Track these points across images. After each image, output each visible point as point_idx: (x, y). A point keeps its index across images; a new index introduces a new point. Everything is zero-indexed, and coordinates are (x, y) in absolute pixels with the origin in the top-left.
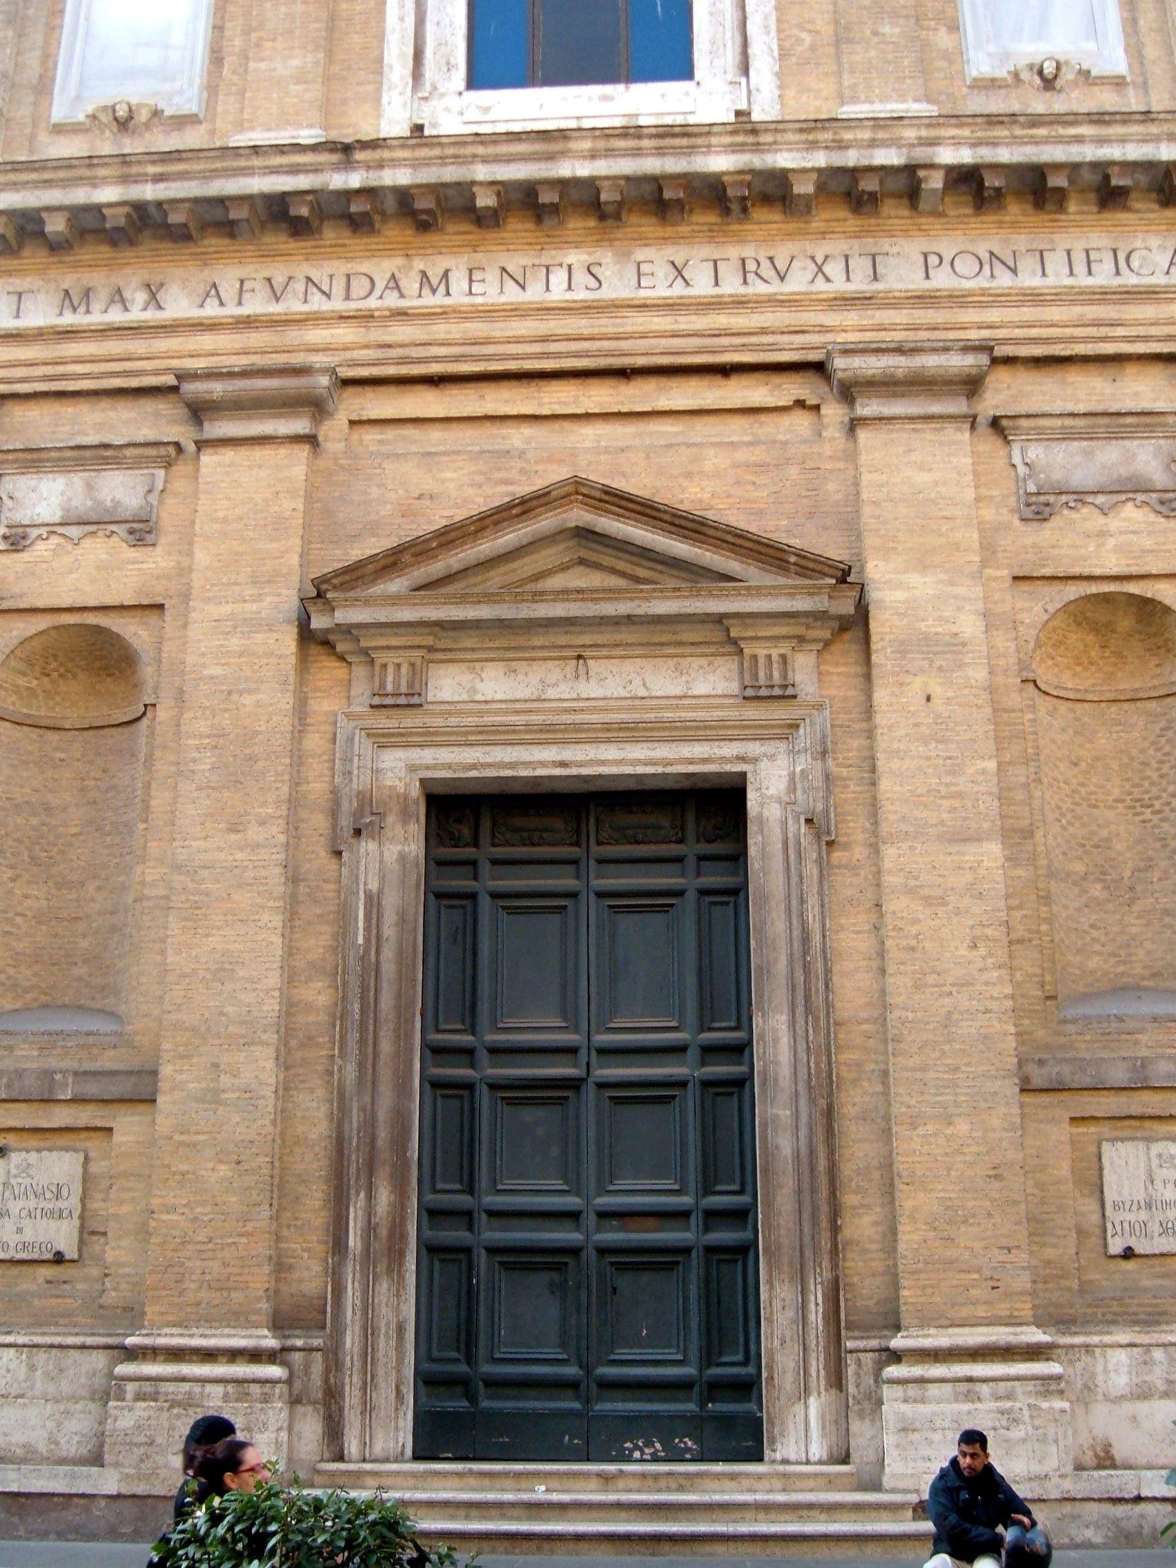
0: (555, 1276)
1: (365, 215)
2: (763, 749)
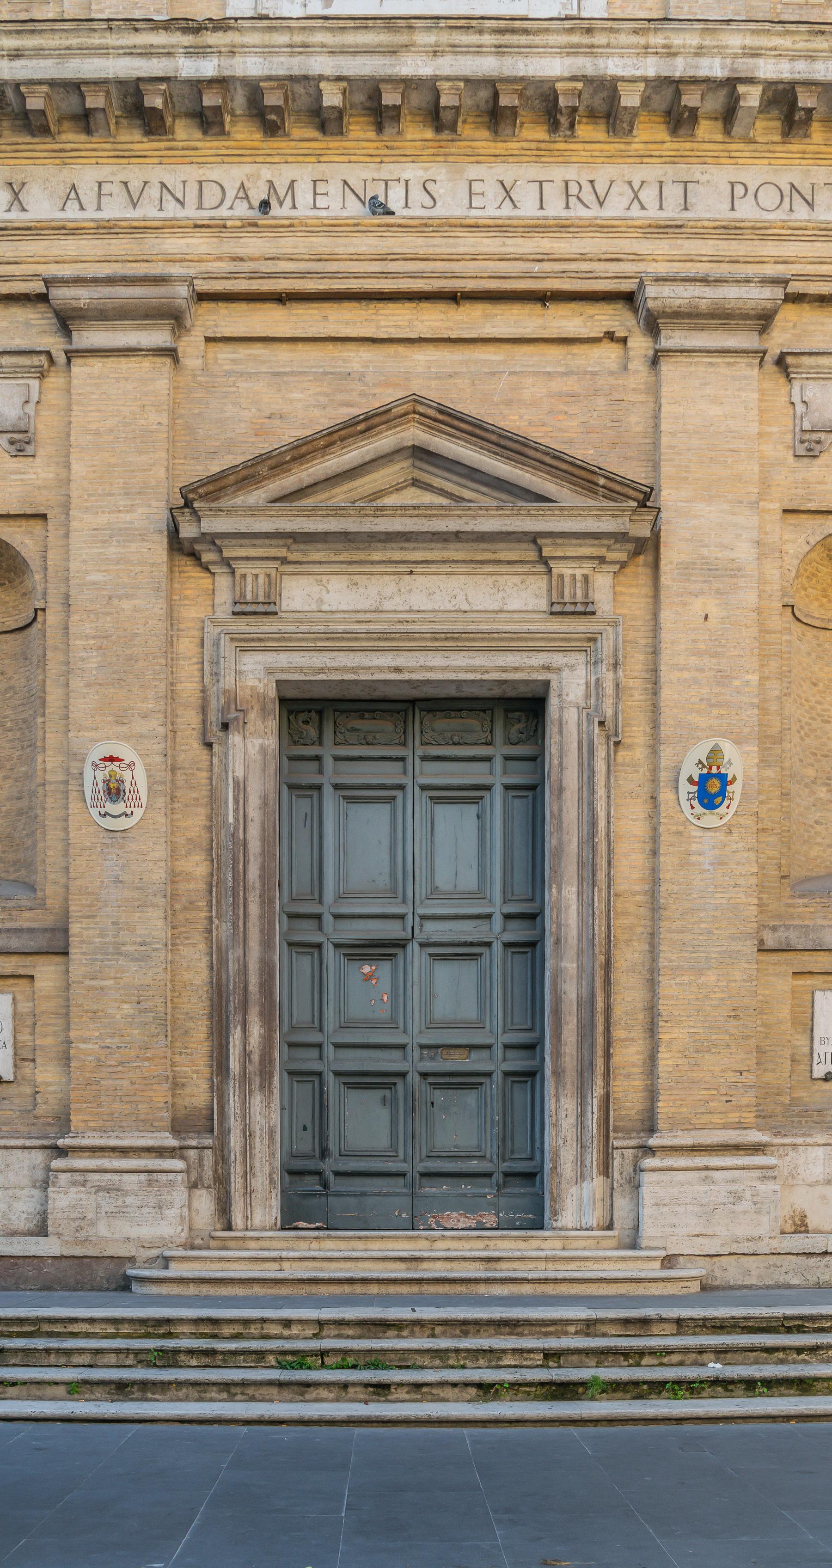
0: (387, 1093)
1: (217, 110)
2: (565, 660)
